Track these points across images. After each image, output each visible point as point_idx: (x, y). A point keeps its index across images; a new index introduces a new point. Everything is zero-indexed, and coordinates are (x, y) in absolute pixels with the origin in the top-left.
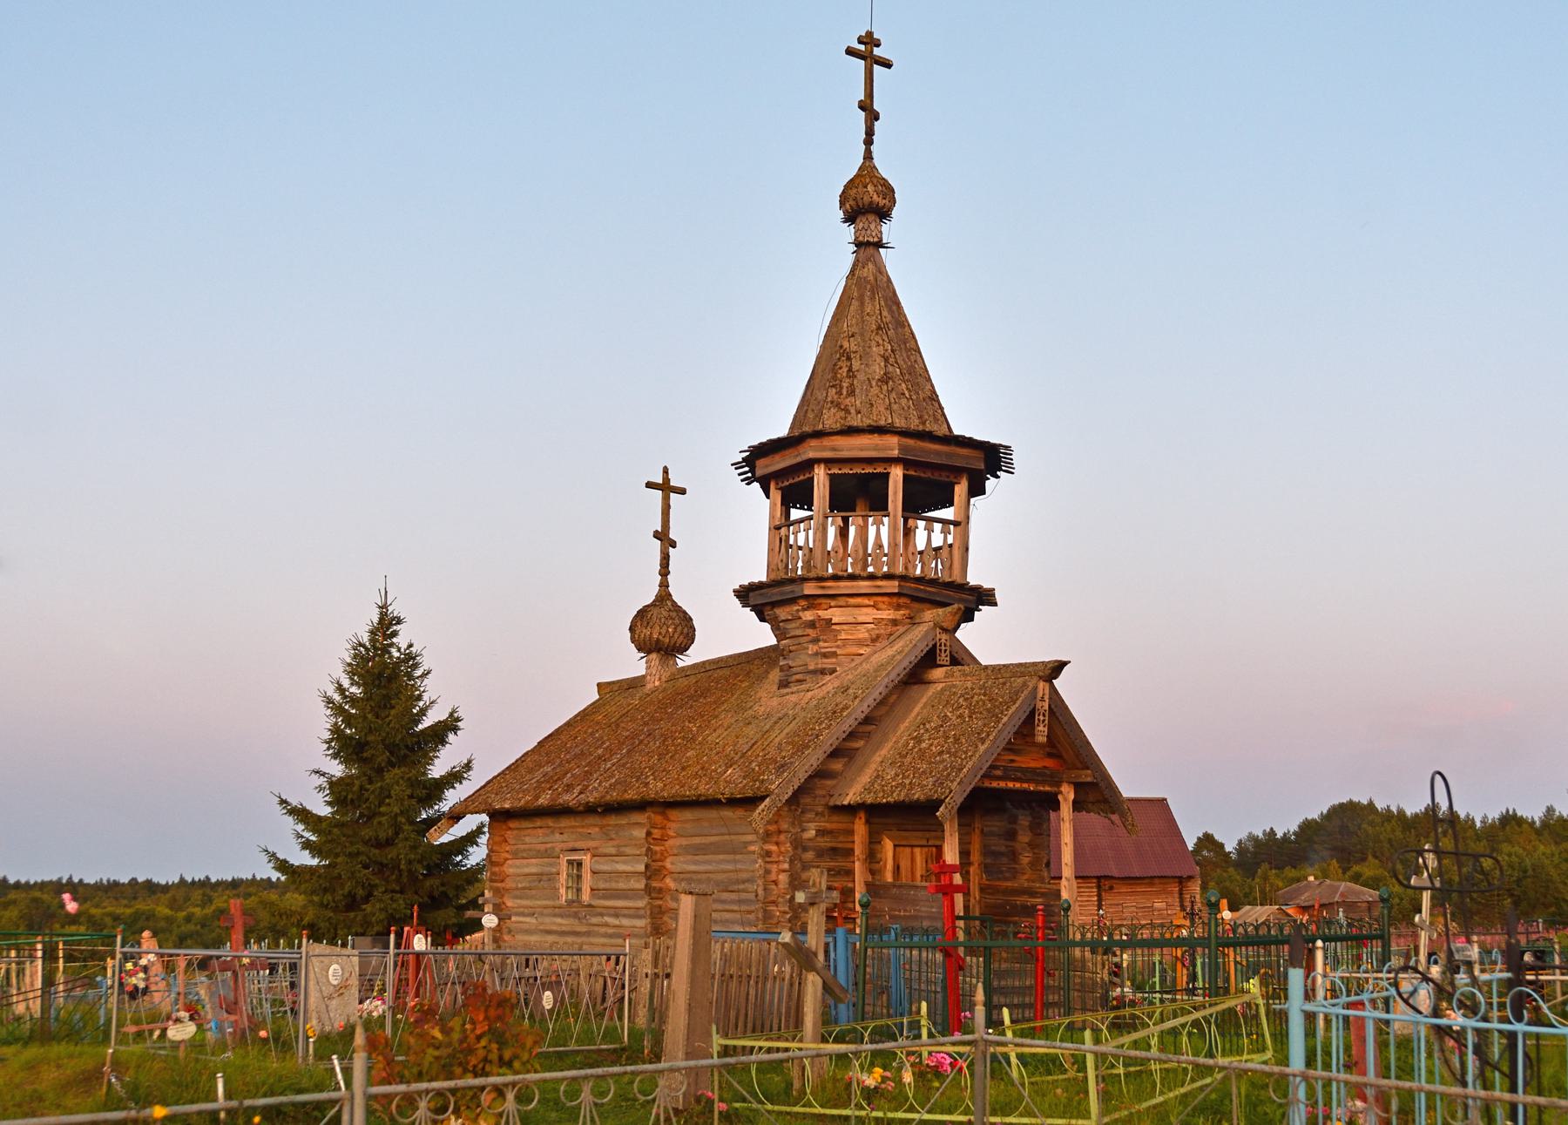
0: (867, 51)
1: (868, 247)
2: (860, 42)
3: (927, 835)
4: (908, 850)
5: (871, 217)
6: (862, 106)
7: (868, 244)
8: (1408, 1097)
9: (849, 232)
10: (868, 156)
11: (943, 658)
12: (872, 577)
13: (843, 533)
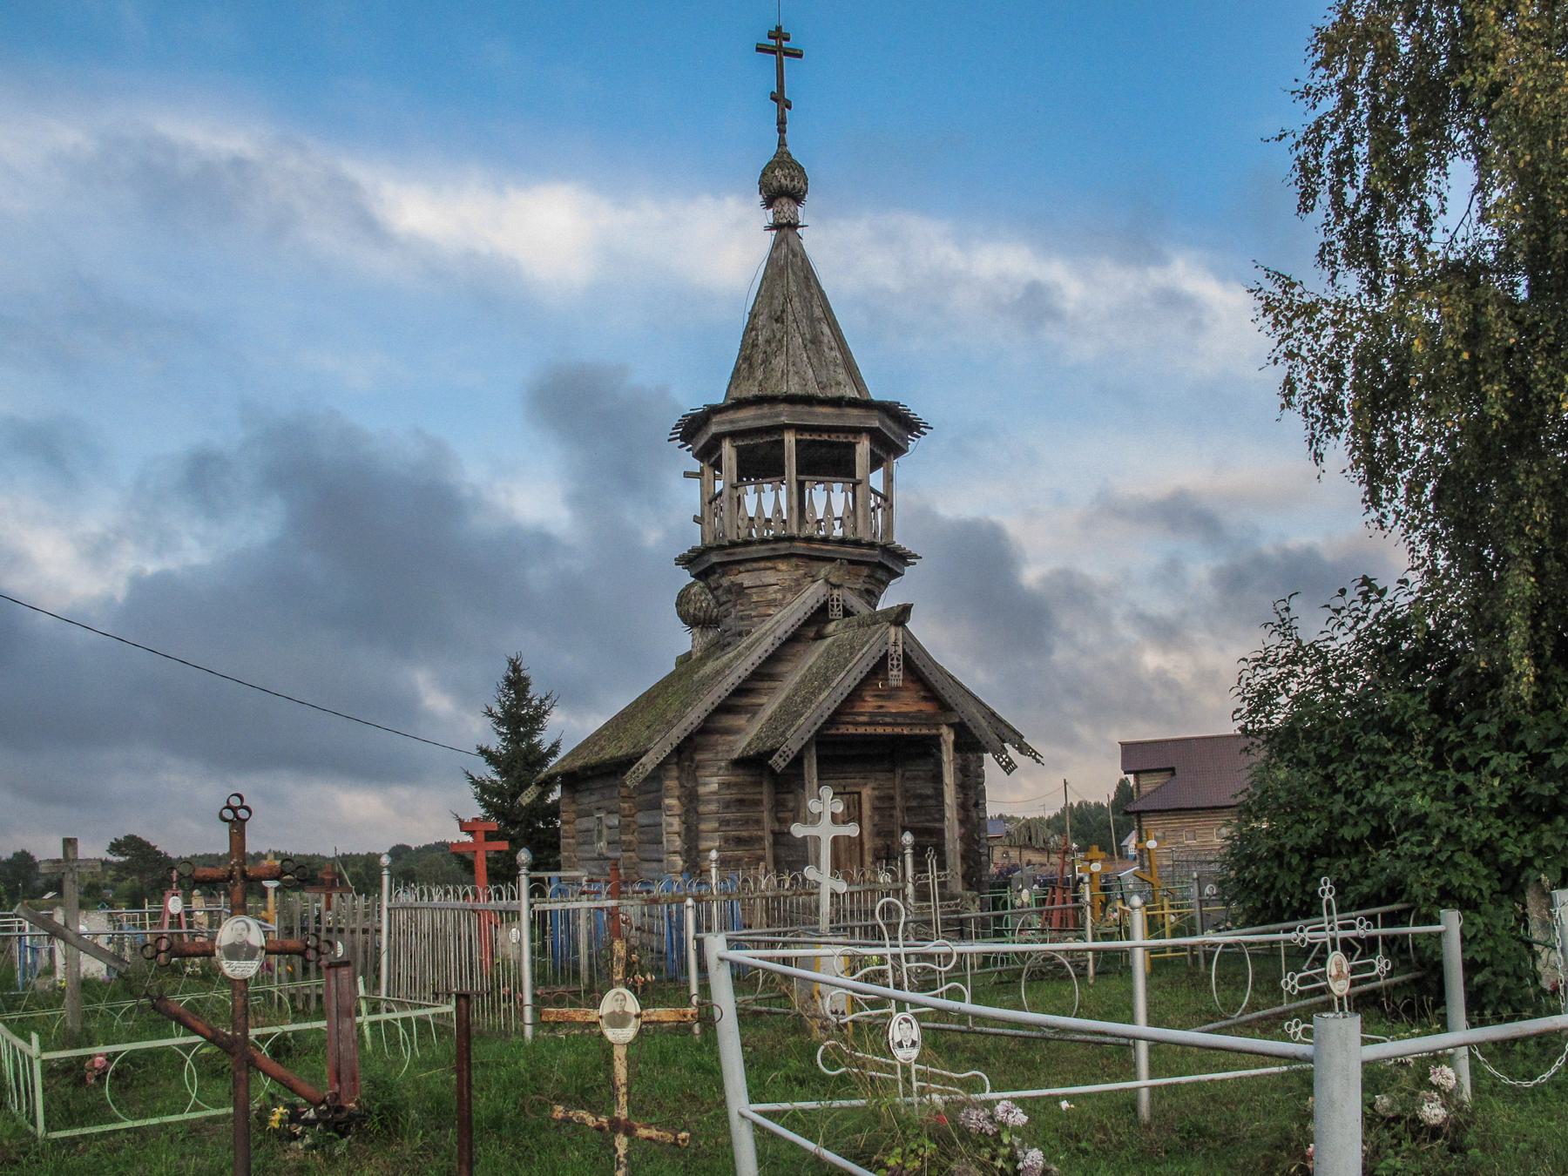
0: (778, 46)
1: (785, 228)
3: (843, 782)
5: (784, 200)
9: (768, 216)
10: (782, 143)
11: (836, 612)
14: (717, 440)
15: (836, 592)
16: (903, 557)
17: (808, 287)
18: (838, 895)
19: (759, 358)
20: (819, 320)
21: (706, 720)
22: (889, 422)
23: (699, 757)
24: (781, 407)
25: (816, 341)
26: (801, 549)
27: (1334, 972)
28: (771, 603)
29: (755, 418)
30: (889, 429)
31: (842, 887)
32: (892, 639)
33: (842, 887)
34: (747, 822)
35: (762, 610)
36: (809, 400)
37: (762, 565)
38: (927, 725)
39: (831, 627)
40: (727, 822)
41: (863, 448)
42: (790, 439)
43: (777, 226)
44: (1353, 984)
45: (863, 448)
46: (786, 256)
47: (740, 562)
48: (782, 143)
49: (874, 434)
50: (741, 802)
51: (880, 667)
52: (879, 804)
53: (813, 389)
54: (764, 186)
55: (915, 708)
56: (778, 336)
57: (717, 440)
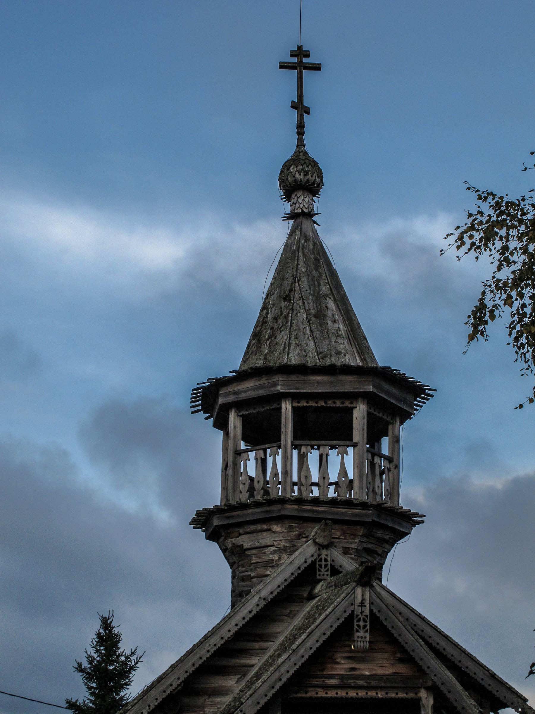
0: (300, 62)
1: (301, 217)
2: (292, 56)
5: (299, 193)
7: (303, 214)
10: (300, 144)
12: (257, 504)
13: (262, 464)
14: (226, 408)
15: (324, 552)
17: (317, 268)
19: (267, 333)
20: (326, 296)
21: (186, 681)
22: (386, 386)
24: (279, 378)
26: (300, 513)
28: (269, 564)
30: (387, 392)
32: (359, 599)
35: (260, 571)
36: (302, 370)
37: (259, 527)
38: (406, 689)
41: (360, 412)
42: (287, 407)
43: (293, 216)
45: (360, 412)
46: (299, 241)
47: (240, 525)
48: (300, 144)
49: (371, 399)
51: (345, 630)
53: (312, 360)
54: (282, 182)
55: (389, 671)
56: (285, 313)
57: (226, 408)
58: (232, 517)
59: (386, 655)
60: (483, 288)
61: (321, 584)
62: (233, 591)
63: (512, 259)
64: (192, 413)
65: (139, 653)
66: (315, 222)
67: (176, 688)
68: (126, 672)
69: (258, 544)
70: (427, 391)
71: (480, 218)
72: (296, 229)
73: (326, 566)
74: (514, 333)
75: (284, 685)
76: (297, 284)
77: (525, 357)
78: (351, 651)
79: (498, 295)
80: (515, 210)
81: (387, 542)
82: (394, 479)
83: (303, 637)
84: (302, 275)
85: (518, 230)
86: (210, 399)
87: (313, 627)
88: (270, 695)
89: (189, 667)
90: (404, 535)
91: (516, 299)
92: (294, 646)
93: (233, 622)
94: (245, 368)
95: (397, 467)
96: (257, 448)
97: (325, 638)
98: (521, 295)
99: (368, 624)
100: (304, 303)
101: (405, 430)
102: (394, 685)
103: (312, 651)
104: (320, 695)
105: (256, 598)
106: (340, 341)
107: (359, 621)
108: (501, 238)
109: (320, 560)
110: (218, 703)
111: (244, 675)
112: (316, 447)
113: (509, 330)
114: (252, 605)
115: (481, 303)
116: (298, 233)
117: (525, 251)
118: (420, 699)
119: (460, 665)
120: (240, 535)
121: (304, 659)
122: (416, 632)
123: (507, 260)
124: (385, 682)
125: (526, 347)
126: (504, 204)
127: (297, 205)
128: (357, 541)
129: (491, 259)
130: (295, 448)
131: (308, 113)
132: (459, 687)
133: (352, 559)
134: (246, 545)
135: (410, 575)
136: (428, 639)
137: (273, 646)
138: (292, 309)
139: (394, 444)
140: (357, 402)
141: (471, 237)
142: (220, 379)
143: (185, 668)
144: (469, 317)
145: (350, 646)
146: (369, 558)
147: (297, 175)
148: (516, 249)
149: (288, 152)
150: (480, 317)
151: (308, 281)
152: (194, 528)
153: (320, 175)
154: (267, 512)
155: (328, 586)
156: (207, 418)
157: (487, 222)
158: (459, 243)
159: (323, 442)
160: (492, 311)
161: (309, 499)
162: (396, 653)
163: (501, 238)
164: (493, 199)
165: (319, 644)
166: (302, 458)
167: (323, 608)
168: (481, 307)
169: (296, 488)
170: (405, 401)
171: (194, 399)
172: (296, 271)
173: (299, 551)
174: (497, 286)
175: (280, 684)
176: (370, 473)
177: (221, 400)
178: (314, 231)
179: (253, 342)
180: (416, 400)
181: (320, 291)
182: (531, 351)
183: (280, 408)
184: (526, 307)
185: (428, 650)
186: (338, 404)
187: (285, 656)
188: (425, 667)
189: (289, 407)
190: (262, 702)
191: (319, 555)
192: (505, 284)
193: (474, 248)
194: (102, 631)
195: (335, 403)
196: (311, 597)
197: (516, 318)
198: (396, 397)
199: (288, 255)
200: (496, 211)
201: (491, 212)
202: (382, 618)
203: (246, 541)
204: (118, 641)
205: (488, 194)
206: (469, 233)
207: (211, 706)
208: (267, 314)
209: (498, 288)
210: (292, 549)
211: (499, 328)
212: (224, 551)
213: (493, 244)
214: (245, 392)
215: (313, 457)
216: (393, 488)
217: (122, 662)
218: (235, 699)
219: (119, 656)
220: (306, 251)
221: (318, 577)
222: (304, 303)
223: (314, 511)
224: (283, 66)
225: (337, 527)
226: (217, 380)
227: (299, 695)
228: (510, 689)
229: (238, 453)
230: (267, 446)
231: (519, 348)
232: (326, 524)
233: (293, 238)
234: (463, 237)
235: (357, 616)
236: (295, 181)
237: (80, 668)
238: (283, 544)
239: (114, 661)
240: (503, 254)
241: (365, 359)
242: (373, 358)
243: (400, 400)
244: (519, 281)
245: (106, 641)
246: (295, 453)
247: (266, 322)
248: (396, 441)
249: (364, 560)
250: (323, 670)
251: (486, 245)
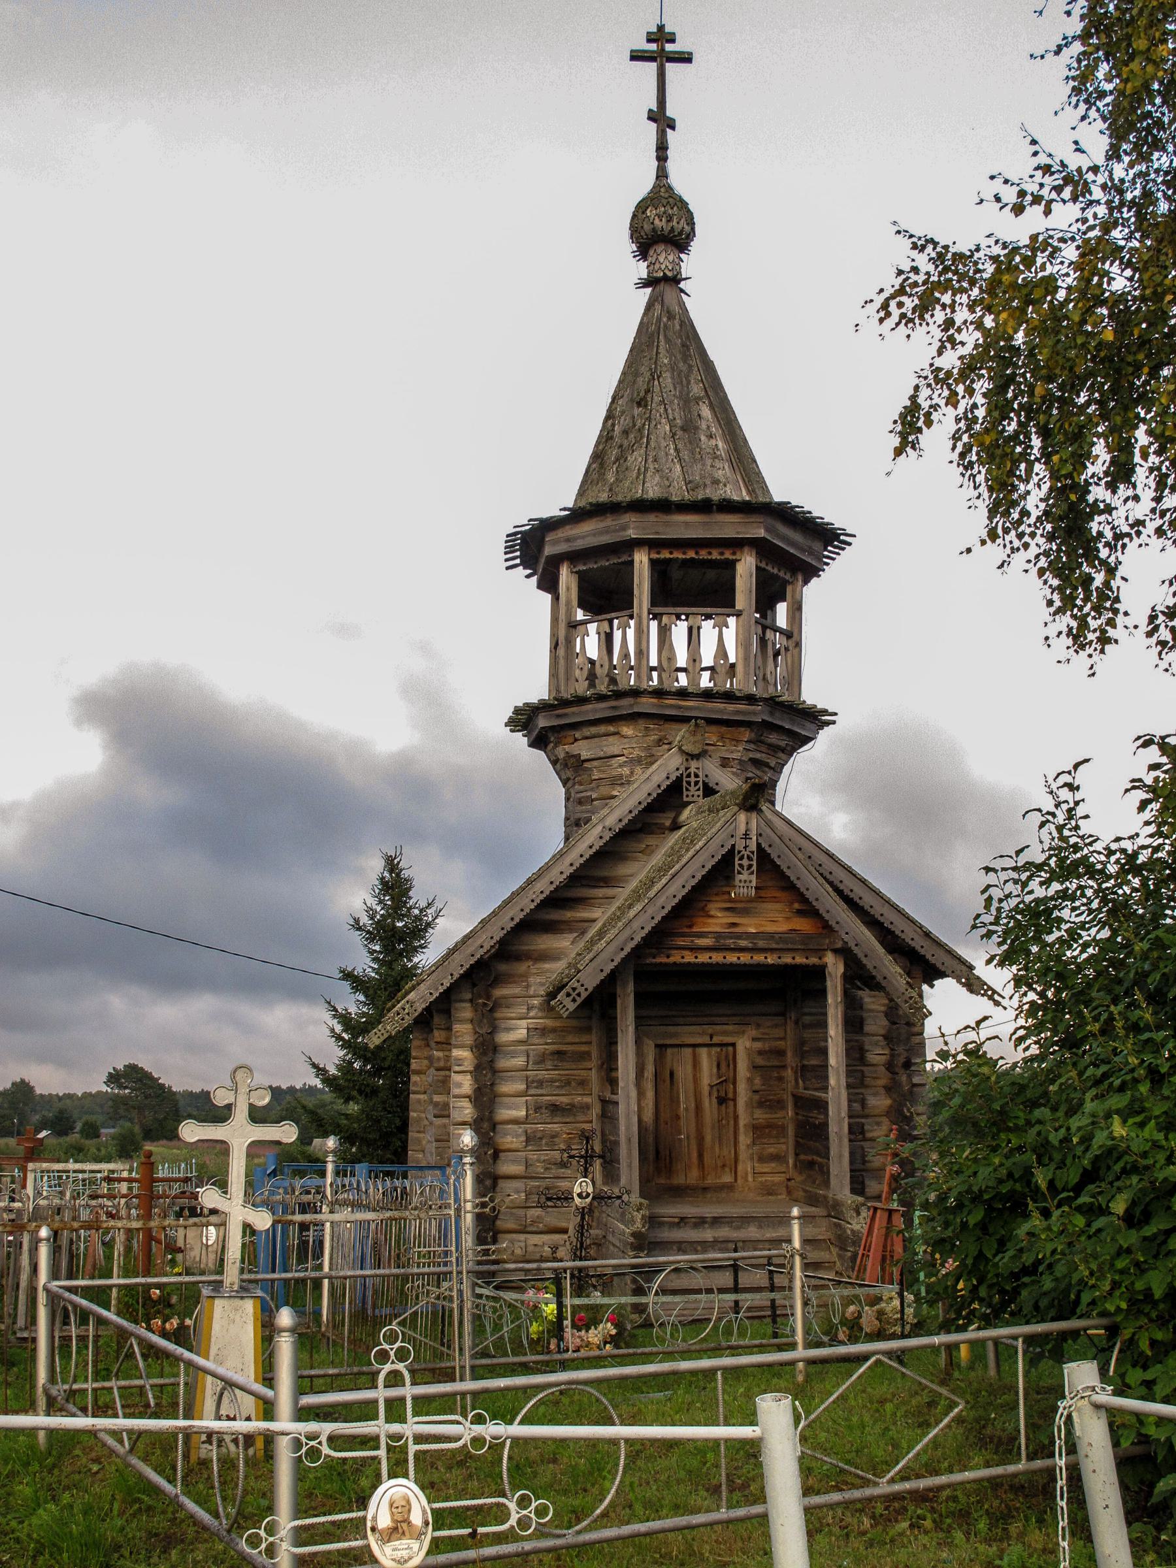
0: (661, 51)
1: (663, 284)
2: (649, 41)
3: (709, 1029)
4: (689, 1050)
5: (660, 248)
6: (652, 117)
7: (665, 279)
8: (269, 1439)
9: (641, 270)
10: (662, 173)
11: (693, 793)
12: (601, 698)
13: (608, 639)
14: (555, 562)
15: (694, 765)
16: (816, 718)
17: (686, 357)
18: (253, 1232)
20: (697, 400)
21: (502, 942)
23: (499, 992)
24: (630, 518)
25: (690, 427)
26: (660, 708)
27: (384, 1522)
29: (595, 534)
31: (263, 1220)
33: (263, 1220)
34: (568, 1083)
35: (605, 790)
36: (663, 506)
37: (602, 729)
38: (807, 952)
39: (686, 813)
40: (540, 1083)
41: (746, 567)
42: (641, 560)
44: (437, 1546)
45: (746, 567)
46: (659, 319)
48: (662, 173)
49: (761, 547)
50: (559, 1054)
51: (722, 870)
52: (760, 1061)
53: (679, 492)
54: (636, 231)
55: (783, 927)
56: (639, 423)
57: (555, 562)
58: (565, 715)
59: (778, 906)
60: (916, 381)
61: (690, 807)
62: (567, 819)
63: (959, 338)
64: (507, 568)
65: (438, 904)
66: (682, 291)
67: (488, 951)
68: (420, 930)
69: (601, 754)
70: (842, 537)
71: (914, 277)
72: (656, 300)
73: (696, 783)
74: (960, 446)
75: (638, 947)
76: (656, 382)
77: (974, 482)
78: (731, 901)
79: (937, 393)
80: (965, 265)
81: (783, 750)
82: (793, 662)
83: (664, 881)
84: (664, 369)
85: (969, 296)
86: (532, 547)
87: (677, 867)
88: (617, 960)
89: (507, 922)
90: (806, 740)
91: (964, 397)
92: (651, 894)
93: (568, 860)
94: (582, 504)
95: (798, 645)
96: (600, 617)
97: (694, 882)
98: (970, 392)
99: (754, 863)
100: (666, 410)
101: (813, 593)
102: (790, 946)
103: (676, 900)
104: (686, 960)
105: (599, 828)
106: (718, 464)
107: (741, 859)
108: (944, 306)
109: (689, 776)
110: (548, 971)
111: (583, 933)
112: (683, 617)
113: (952, 442)
114: (592, 838)
115: (912, 403)
116: (658, 307)
117: (979, 325)
118: (825, 966)
119: (881, 919)
120: (576, 740)
121: (666, 911)
122: (821, 875)
123: (951, 340)
124: (777, 943)
125: (976, 466)
126: (949, 256)
127: (657, 266)
128: (740, 748)
129: (928, 339)
130: (653, 619)
131: (673, 128)
132: (881, 950)
133: (734, 773)
134: (585, 755)
135: (812, 797)
136: (839, 885)
137: (622, 894)
138: (649, 419)
139: (793, 613)
140: (742, 552)
141: (900, 305)
142: (547, 519)
143: (500, 924)
144: (895, 422)
145: (729, 894)
146: (758, 773)
147: (657, 222)
148: (965, 322)
149: (645, 183)
150: (910, 425)
151: (672, 378)
152: (512, 731)
153: (691, 223)
154: (614, 708)
155: (699, 812)
156: (528, 576)
157: (924, 283)
158: (882, 314)
159: (694, 610)
160: (928, 415)
161: (673, 690)
162: (792, 903)
163: (944, 306)
164: (934, 249)
165: (686, 890)
166: (664, 633)
167: (692, 841)
168: (913, 408)
169: (655, 674)
170: (811, 553)
171: (509, 549)
172: (656, 363)
173: (658, 763)
174: (936, 377)
175: (632, 944)
176: (759, 654)
177: (548, 550)
178: (682, 305)
179: (594, 466)
180: (826, 549)
181: (689, 392)
182: (983, 471)
183: (633, 561)
184: (977, 408)
185: (837, 899)
186: (715, 555)
187: (638, 907)
188: (832, 923)
189: (645, 560)
190: (607, 970)
191: (687, 769)
192: (949, 374)
193: (904, 321)
194: (386, 874)
195: (710, 553)
196: (676, 826)
197: (962, 424)
198: (797, 546)
199: (644, 339)
200: (937, 267)
201: (931, 268)
202: (774, 856)
203: (584, 750)
204: (410, 889)
205: (927, 241)
206: (898, 299)
207: (537, 974)
208: (613, 425)
209: (937, 380)
210: (649, 760)
211: (938, 439)
212: (554, 763)
213: (932, 316)
214: (583, 537)
215: (679, 632)
216: (793, 672)
217: (416, 916)
218: (570, 965)
219: (411, 908)
220: (670, 334)
221: (685, 799)
222: (666, 410)
223: (680, 707)
224: (636, 56)
225: (714, 728)
226: (541, 520)
227: (658, 960)
228: (950, 953)
229: (573, 625)
230: (613, 615)
231: (966, 468)
232: (696, 725)
233: (651, 314)
234: (888, 306)
235: (739, 852)
236: (654, 230)
237: (357, 926)
238: (636, 752)
239: (403, 916)
240: (946, 330)
241: (754, 491)
242: (765, 489)
243: (803, 550)
244: (969, 369)
245: (392, 888)
246: (654, 625)
247: (612, 438)
248: (796, 610)
249: (750, 775)
250: (690, 927)
251: (922, 318)
